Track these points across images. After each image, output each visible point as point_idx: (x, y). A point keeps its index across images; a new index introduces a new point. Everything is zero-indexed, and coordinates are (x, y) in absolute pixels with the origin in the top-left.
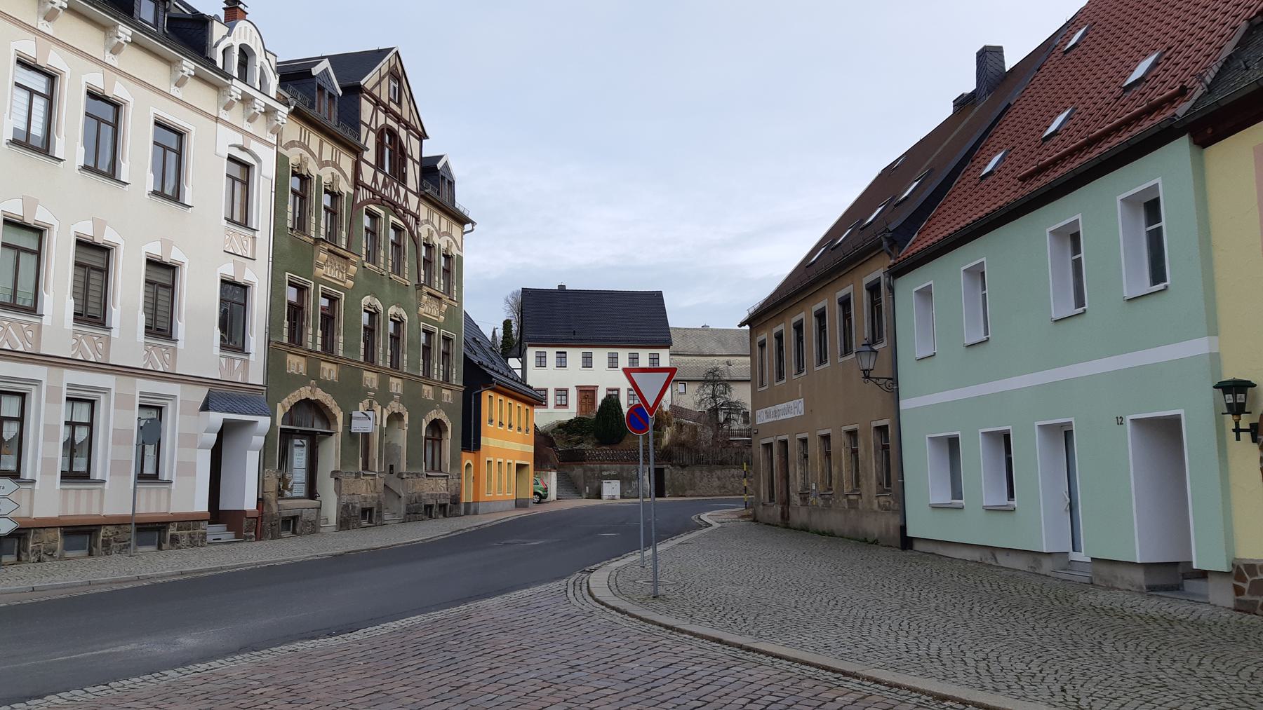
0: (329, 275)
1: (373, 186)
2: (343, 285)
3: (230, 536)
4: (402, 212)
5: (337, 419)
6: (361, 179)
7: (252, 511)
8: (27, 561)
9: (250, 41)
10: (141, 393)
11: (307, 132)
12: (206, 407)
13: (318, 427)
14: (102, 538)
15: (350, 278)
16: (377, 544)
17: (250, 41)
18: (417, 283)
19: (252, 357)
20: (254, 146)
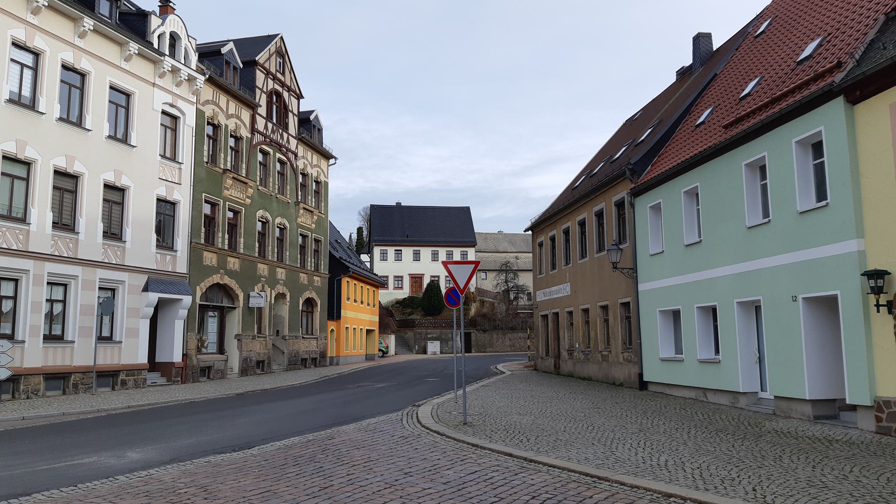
0: (234, 195)
1: (265, 132)
2: (243, 202)
3: (163, 381)
4: (285, 150)
5: (239, 298)
6: (256, 127)
7: (178, 363)
8: (19, 398)
9: (178, 29)
10: (100, 279)
11: (218, 94)
12: (146, 289)
13: (226, 303)
14: (72, 382)
15: (248, 197)
16: (267, 386)
17: (178, 29)
18: (296, 201)
19: (179, 254)
20: (180, 104)
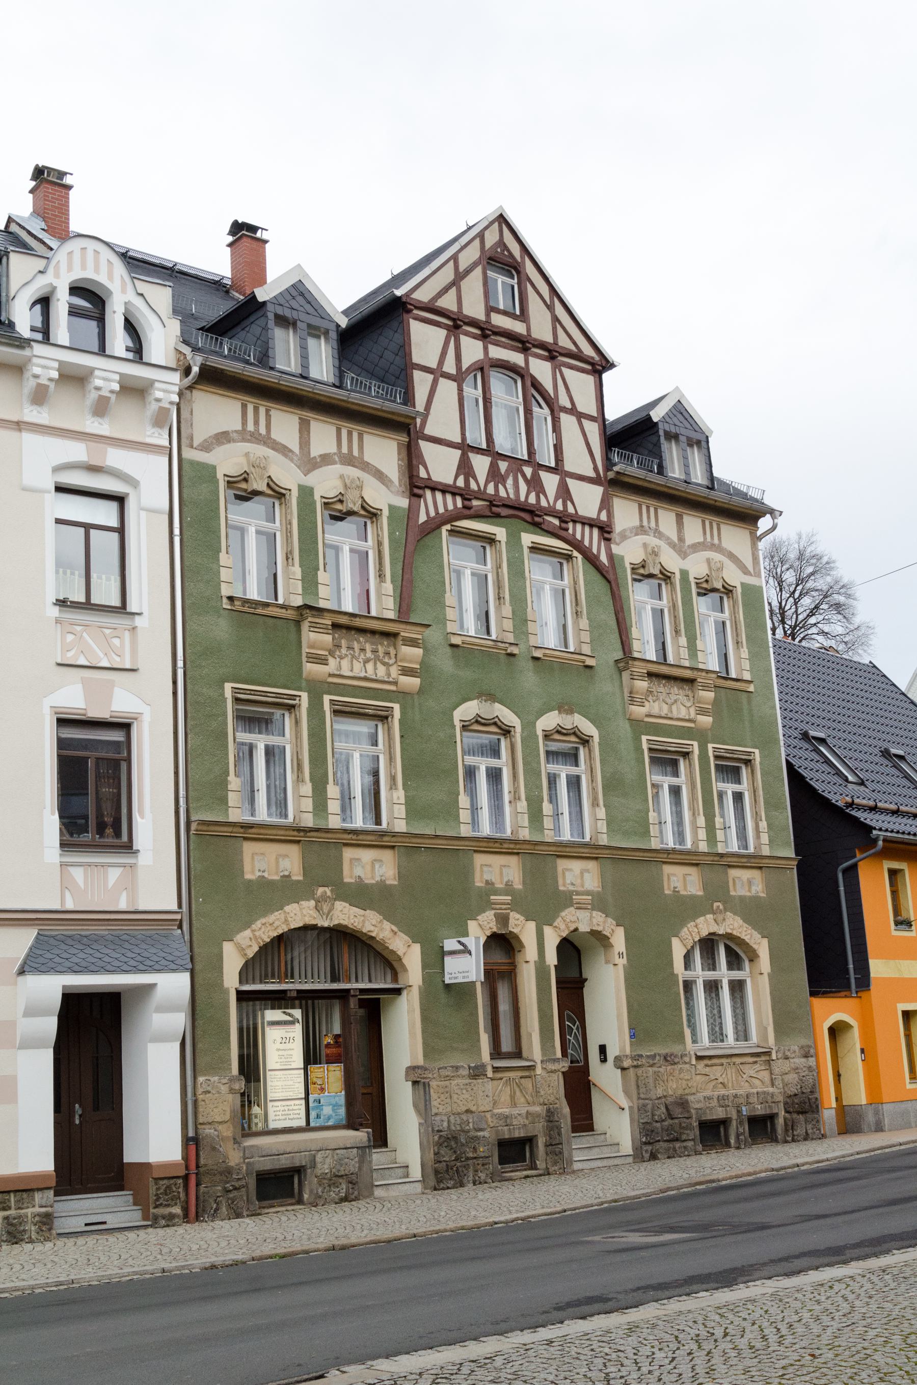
1: (461, 482)
2: (393, 688)
4: (556, 522)
5: (405, 961)
6: (423, 474)
9: (110, 277)
11: (262, 411)
12: (21, 972)
15: (407, 672)
16: (484, 1217)
17: (97, 270)
18: (619, 655)
20: (115, 458)
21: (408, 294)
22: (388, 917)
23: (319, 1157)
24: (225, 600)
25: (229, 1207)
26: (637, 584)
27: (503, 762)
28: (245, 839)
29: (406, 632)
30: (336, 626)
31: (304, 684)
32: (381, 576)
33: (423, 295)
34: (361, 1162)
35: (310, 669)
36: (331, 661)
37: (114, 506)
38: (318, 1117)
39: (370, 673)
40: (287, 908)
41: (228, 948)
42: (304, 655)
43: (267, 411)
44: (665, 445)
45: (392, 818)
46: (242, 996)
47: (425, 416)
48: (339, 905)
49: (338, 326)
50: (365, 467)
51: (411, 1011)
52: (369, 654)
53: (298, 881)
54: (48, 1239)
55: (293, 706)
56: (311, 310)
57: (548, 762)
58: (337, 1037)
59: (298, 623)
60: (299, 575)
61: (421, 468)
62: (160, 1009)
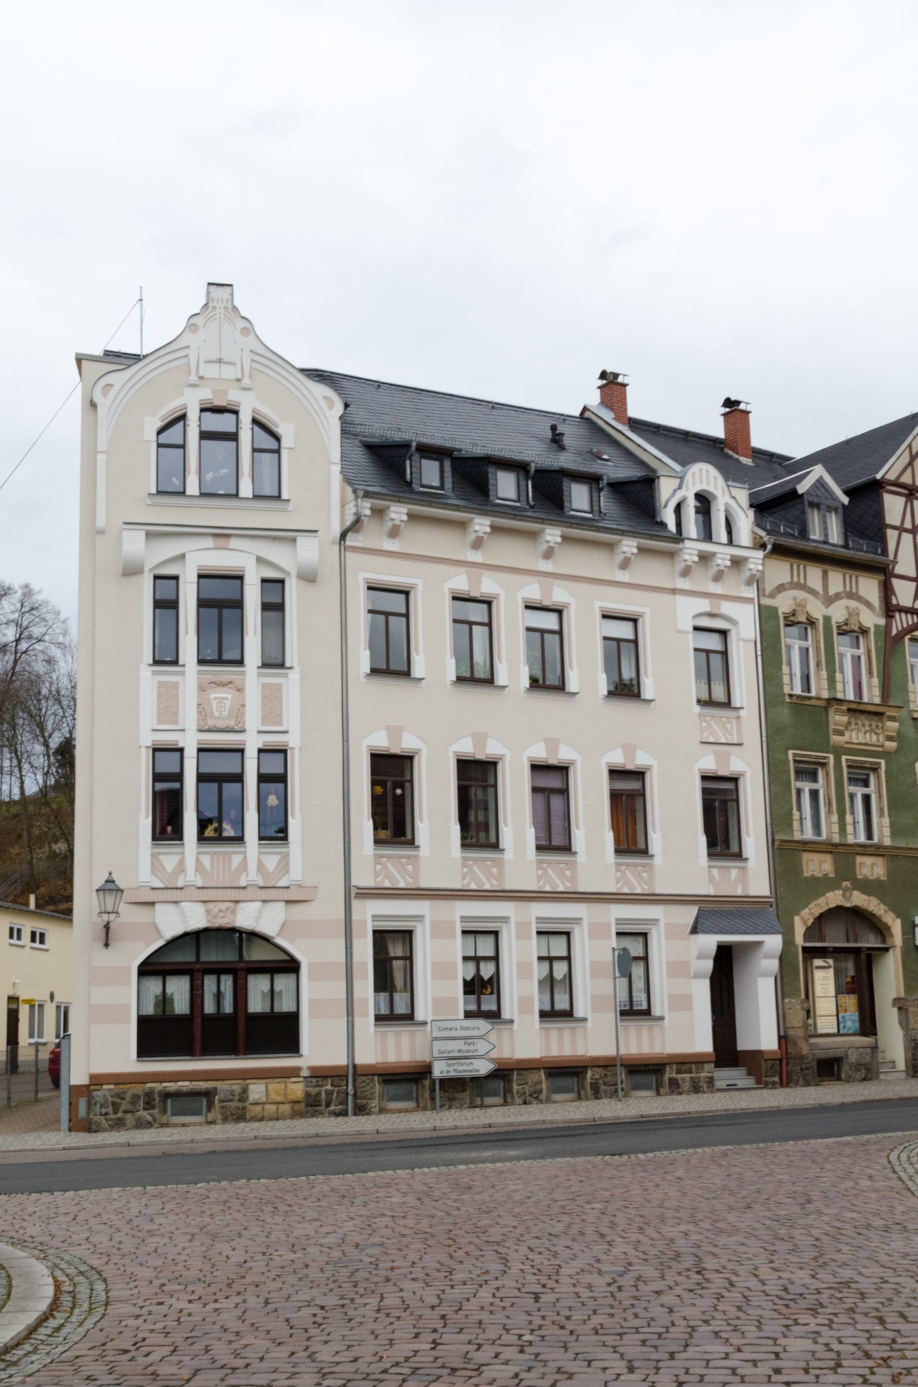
0: (856, 741)
2: (880, 749)
3: (750, 1082)
5: (892, 930)
6: (894, 602)
7: (772, 1052)
8: (513, 1104)
9: (716, 487)
10: (616, 919)
11: (802, 567)
12: (694, 931)
13: (870, 941)
14: (589, 1080)
15: (890, 738)
17: (708, 483)
19: (751, 864)
20: (727, 608)
21: (883, 477)
22: (883, 901)
23: (850, 1052)
24: (787, 697)
25: (804, 1079)
26: (841, 637)
27: (820, 786)
28: (804, 851)
29: (890, 713)
30: (849, 710)
31: (831, 750)
32: (870, 673)
33: (891, 476)
34: (872, 1057)
35: (836, 739)
36: (846, 733)
37: (630, 625)
38: (844, 1027)
39: (868, 741)
40: (828, 895)
41: (797, 919)
42: (831, 730)
43: (805, 567)
44: (808, 510)
45: (881, 836)
46: (805, 950)
47: (895, 562)
48: (856, 893)
49: (843, 505)
50: (860, 599)
51: (896, 962)
52: (867, 728)
53: (832, 878)
54: (712, 1092)
55: (825, 764)
56: (828, 496)
57: (797, 779)
58: (852, 977)
59: (826, 709)
60: (825, 677)
61: (893, 597)
62: (766, 957)
